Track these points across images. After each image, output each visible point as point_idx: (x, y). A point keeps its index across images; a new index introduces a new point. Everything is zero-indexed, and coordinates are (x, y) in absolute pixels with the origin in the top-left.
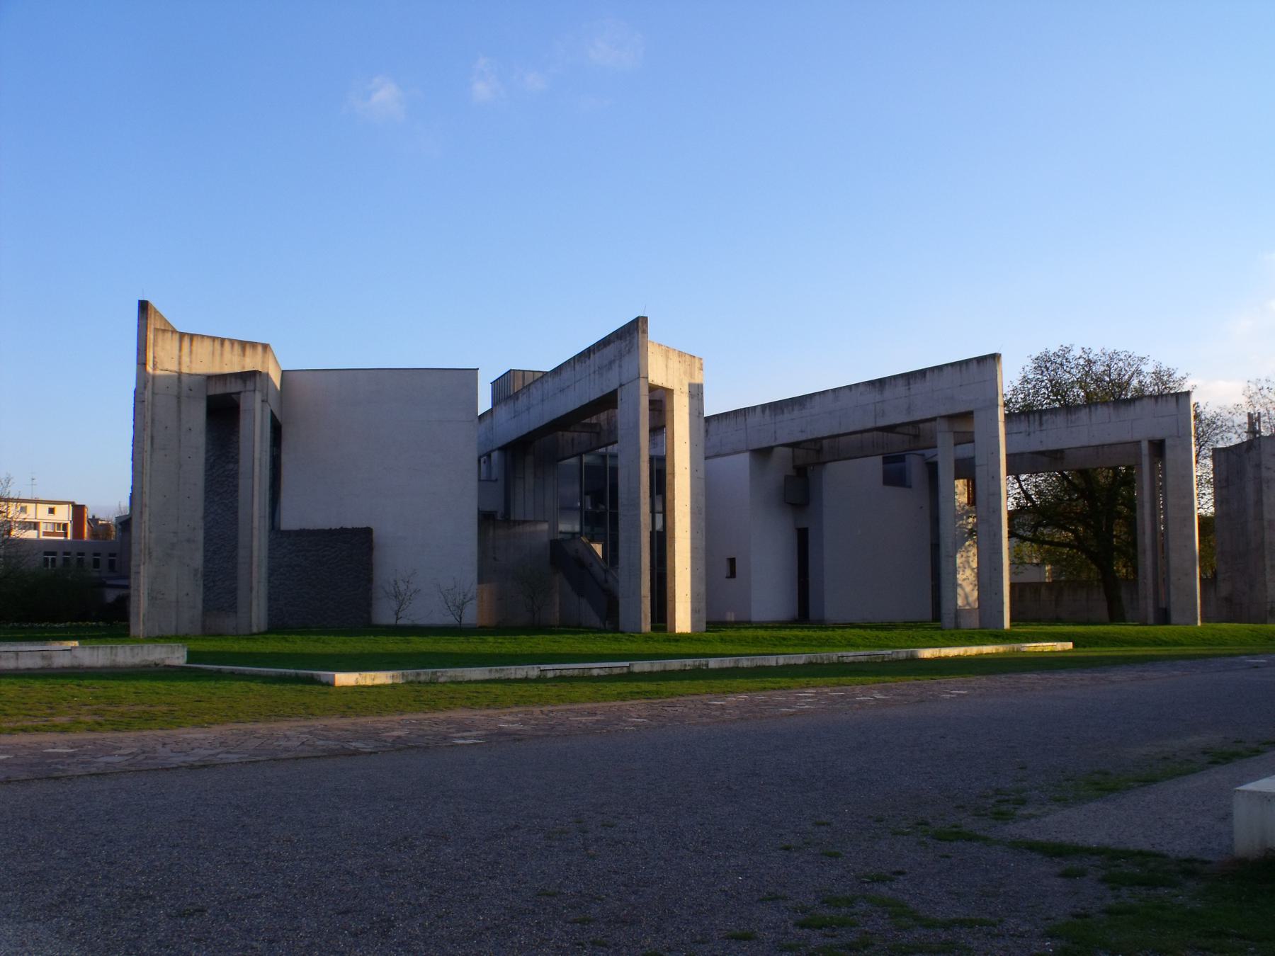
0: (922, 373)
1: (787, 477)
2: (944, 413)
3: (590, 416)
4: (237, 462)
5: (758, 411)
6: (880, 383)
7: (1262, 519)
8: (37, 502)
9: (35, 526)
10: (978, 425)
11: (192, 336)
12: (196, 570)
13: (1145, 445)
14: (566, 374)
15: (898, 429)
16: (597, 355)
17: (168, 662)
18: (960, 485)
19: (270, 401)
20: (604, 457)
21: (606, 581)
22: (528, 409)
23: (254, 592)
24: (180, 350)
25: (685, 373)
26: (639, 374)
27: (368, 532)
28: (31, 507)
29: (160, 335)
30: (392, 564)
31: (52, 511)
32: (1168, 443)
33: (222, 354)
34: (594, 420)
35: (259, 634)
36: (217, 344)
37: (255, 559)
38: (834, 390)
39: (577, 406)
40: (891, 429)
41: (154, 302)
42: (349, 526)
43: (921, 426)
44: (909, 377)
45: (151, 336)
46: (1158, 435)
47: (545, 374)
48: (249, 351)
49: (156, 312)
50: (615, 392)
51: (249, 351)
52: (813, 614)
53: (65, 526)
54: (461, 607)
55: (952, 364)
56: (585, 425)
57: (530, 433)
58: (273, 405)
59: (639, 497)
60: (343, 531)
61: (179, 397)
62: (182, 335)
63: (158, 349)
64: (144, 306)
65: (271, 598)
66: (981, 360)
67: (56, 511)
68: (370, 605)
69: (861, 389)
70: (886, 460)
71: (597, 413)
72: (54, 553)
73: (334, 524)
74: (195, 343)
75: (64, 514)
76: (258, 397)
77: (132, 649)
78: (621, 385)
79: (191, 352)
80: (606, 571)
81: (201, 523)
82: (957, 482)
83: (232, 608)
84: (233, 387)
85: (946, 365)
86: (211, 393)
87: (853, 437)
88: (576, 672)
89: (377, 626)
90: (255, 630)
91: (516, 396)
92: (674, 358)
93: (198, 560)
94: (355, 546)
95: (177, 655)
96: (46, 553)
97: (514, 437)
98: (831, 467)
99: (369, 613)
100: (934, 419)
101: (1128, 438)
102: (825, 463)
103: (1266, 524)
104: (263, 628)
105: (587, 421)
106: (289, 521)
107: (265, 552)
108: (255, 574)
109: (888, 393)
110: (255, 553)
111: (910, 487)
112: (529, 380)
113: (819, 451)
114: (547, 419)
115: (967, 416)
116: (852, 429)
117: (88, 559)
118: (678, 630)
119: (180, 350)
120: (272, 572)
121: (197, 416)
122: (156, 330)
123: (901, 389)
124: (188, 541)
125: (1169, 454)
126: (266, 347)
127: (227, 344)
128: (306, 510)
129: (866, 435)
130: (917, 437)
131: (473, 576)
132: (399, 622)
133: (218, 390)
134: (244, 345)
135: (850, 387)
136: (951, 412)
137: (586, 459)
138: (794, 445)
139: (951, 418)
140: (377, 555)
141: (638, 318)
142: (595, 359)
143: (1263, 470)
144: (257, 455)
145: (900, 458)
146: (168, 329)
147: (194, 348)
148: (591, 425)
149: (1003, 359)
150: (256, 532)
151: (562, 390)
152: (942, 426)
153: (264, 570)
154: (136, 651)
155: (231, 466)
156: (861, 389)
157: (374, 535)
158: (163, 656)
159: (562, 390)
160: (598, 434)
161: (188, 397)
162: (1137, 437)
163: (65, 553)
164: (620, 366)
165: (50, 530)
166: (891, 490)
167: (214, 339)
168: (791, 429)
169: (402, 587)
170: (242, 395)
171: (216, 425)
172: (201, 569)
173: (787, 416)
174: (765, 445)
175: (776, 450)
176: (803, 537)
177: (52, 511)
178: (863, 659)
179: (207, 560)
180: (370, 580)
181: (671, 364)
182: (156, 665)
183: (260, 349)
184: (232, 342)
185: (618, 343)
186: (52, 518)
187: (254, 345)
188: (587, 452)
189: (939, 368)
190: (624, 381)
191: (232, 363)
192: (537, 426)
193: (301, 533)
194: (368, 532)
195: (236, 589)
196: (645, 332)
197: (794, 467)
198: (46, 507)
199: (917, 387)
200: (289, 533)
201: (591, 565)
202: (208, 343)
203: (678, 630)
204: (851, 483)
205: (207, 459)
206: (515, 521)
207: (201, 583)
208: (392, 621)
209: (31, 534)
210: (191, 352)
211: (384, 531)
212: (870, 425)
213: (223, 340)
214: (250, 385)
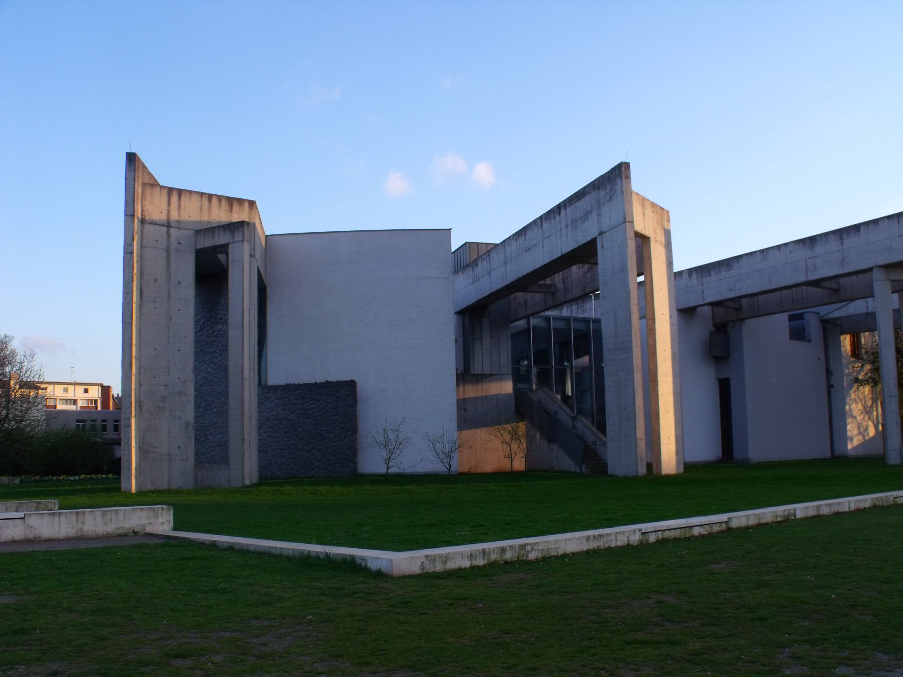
0: (856, 228)
1: (711, 333)
3: (544, 278)
4: (226, 323)
6: (811, 241)
8: (75, 384)
9: (75, 402)
11: (180, 192)
12: (187, 423)
14: (529, 234)
16: (569, 209)
17: (149, 529)
18: (569, 391)
19: (257, 256)
20: (548, 319)
21: (575, 428)
22: (489, 273)
23: (246, 446)
24: (169, 204)
25: (657, 222)
26: (626, 220)
27: (352, 384)
28: (71, 388)
29: (148, 189)
30: (376, 416)
31: (86, 391)
33: (209, 209)
34: (548, 281)
35: (252, 486)
36: (205, 200)
37: (246, 410)
38: (762, 251)
41: (143, 157)
42: (334, 380)
43: (841, 280)
44: (841, 233)
45: (139, 189)
48: (236, 207)
49: (144, 167)
50: (594, 241)
51: (236, 207)
52: (738, 455)
53: (96, 401)
54: (449, 456)
56: (541, 286)
58: (259, 262)
59: (630, 341)
60: (328, 384)
61: (167, 250)
62: (170, 190)
63: (147, 203)
64: (132, 159)
65: (261, 451)
67: (89, 391)
68: (355, 455)
69: (791, 247)
70: (791, 318)
72: (84, 421)
74: (183, 198)
75: (95, 393)
76: (246, 246)
77: (104, 514)
78: (601, 233)
79: (179, 206)
80: (573, 418)
81: (191, 376)
82: (842, 338)
83: (224, 459)
84: (221, 239)
86: (200, 246)
88: (677, 533)
89: (363, 476)
90: (247, 482)
91: (475, 263)
93: (189, 412)
94: (335, 404)
95: (160, 519)
96: (78, 421)
99: (355, 463)
100: (870, 270)
102: (744, 320)
104: (255, 480)
106: (276, 377)
107: (255, 405)
108: (246, 426)
109: (819, 249)
110: (246, 405)
111: (810, 341)
112: (489, 247)
113: (739, 309)
114: (556, 255)
116: (782, 285)
117: (99, 423)
119: (169, 204)
120: (261, 425)
121: (185, 270)
122: (144, 184)
123: (833, 245)
124: (179, 393)
126: (252, 203)
127: (215, 201)
128: (291, 365)
129: (784, 292)
131: (454, 423)
133: (206, 242)
134: (231, 201)
138: (713, 304)
140: (360, 407)
142: (569, 212)
144: (246, 305)
145: (800, 317)
146: (154, 184)
147: (182, 202)
150: (246, 383)
151: (528, 249)
153: (254, 422)
154: (109, 516)
155: (220, 327)
156: (791, 247)
158: (144, 521)
159: (528, 249)
160: (553, 294)
161: (177, 250)
163: (92, 421)
164: (599, 215)
165: (85, 405)
167: (202, 194)
170: (230, 247)
171: (203, 272)
172: (192, 421)
173: (714, 277)
175: (699, 309)
176: (725, 388)
177: (86, 391)
179: (198, 416)
180: (355, 431)
181: (646, 211)
182: (135, 533)
183: (246, 205)
184: (220, 197)
185: (594, 194)
186: (87, 396)
187: (241, 201)
188: (533, 315)
190: (605, 228)
191: (220, 215)
192: (499, 287)
193: (288, 387)
194: (352, 384)
195: (227, 442)
196: (628, 177)
198: (82, 388)
199: (851, 241)
200: (276, 388)
201: (556, 413)
202: (195, 198)
203: (664, 472)
204: (766, 335)
205: (196, 322)
206: (476, 375)
207: (192, 435)
208: (382, 470)
209: (72, 408)
210: (179, 206)
213: (210, 196)
214: (238, 236)
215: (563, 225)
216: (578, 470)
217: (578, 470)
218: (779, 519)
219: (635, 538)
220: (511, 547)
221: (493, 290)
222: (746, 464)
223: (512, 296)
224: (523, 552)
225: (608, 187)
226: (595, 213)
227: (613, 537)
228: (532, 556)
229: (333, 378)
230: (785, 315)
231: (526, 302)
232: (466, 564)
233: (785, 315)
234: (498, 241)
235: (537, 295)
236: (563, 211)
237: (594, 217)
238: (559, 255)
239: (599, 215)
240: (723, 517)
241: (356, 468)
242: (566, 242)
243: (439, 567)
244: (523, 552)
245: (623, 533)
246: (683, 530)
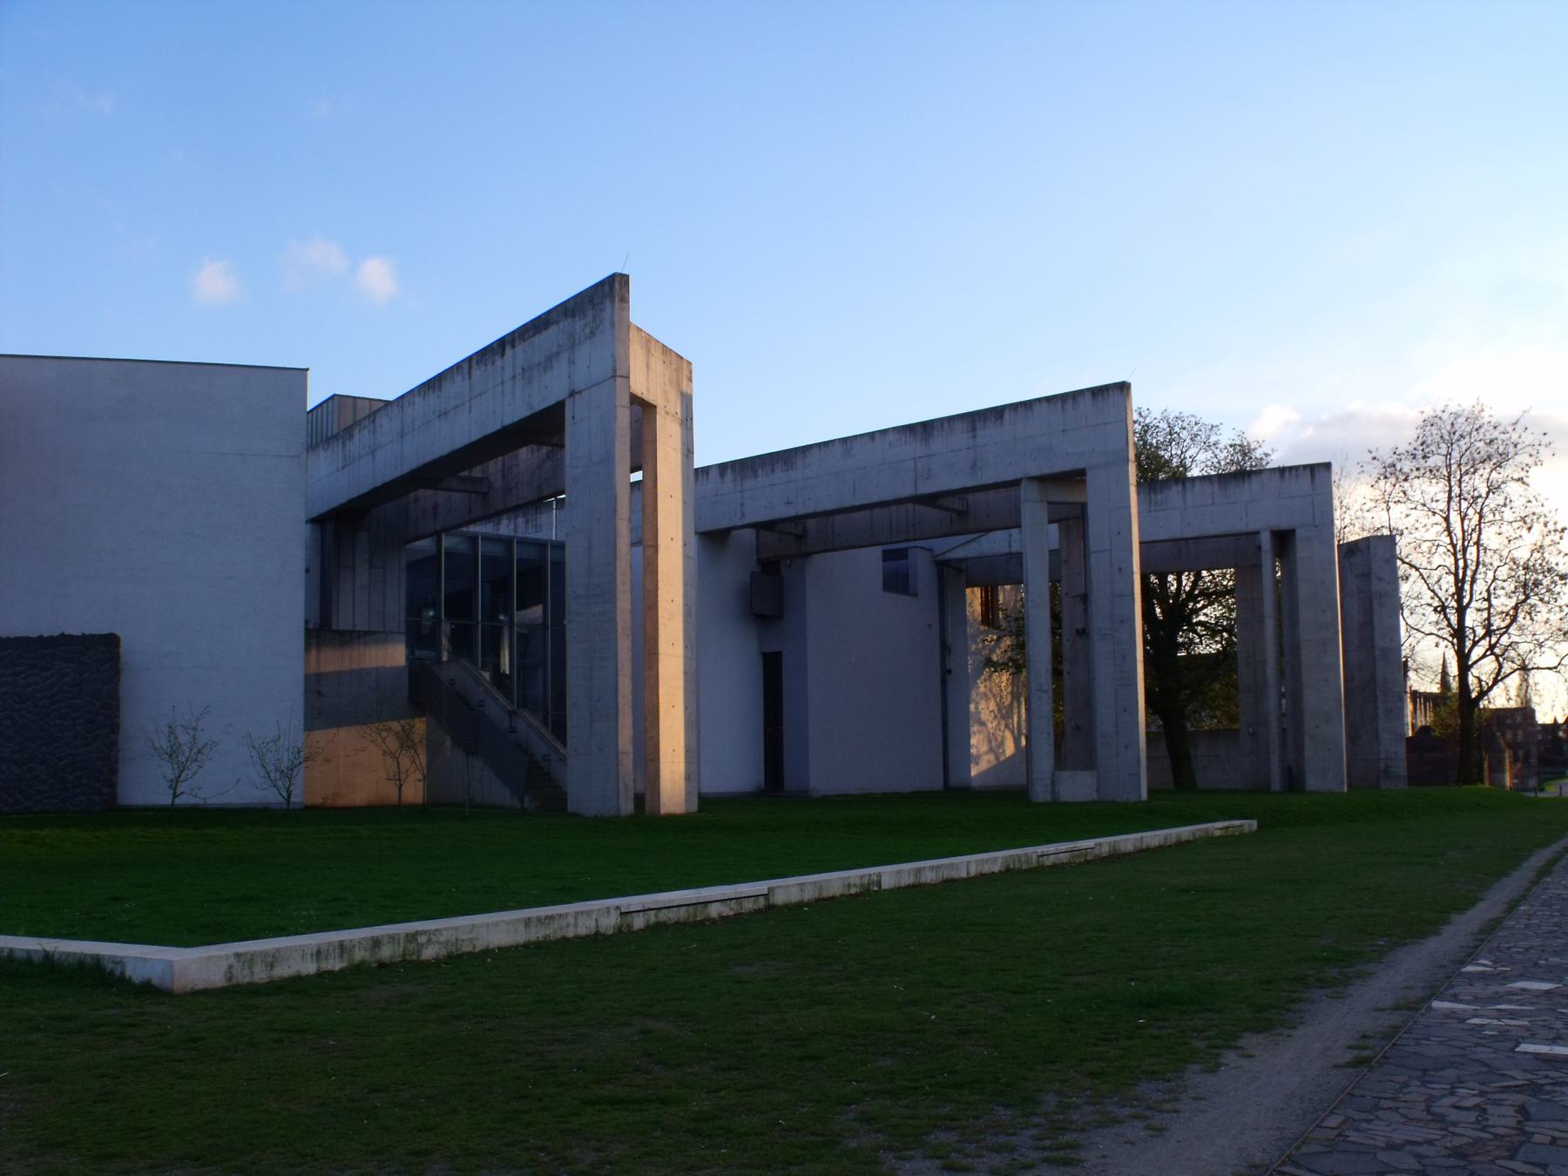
0: (998, 413)
1: (753, 574)
2: (1034, 472)
5: (714, 474)
7: (1373, 646)
10: (1094, 495)
13: (1266, 540)
14: (448, 388)
15: (945, 502)
16: (519, 348)
20: (473, 539)
21: (513, 730)
22: (373, 452)
26: (617, 373)
30: (153, 704)
32: (1300, 534)
34: (477, 472)
38: (844, 440)
39: (475, 436)
40: (931, 500)
43: (970, 497)
44: (974, 419)
46: (1285, 525)
47: (387, 403)
50: (559, 407)
52: (790, 782)
54: (287, 774)
55: (1049, 399)
57: (350, 502)
60: (64, 640)
66: (1098, 392)
68: (114, 771)
69: (891, 437)
70: (888, 556)
71: (483, 460)
73: (49, 629)
78: (572, 394)
80: (511, 714)
85: (1039, 400)
87: (856, 515)
89: (129, 809)
92: (657, 356)
97: (343, 501)
98: (818, 560)
100: (1016, 483)
101: (1241, 527)
102: (809, 554)
103: (1377, 652)
105: (465, 473)
106: (699, 462)
109: (937, 443)
111: (916, 595)
112: (376, 406)
113: (801, 537)
115: (1076, 477)
118: (664, 810)
125: (1301, 551)
129: (878, 512)
130: (962, 514)
131: (298, 718)
132: (178, 801)
135: (872, 435)
136: (1046, 471)
137: (447, 542)
138: (758, 526)
139: (1045, 480)
140: (125, 680)
141: (613, 277)
143: (1374, 581)
145: (902, 554)
148: (473, 480)
149: (1134, 391)
152: (1028, 492)
157: (124, 647)
160: (485, 495)
162: (1252, 527)
164: (572, 362)
166: (892, 598)
168: (768, 502)
169: (184, 738)
174: (724, 524)
176: (772, 669)
178: (1064, 858)
185: (565, 324)
188: (447, 530)
189: (1027, 405)
190: (579, 385)
192: (388, 478)
196: (625, 300)
197: (759, 561)
199: (987, 433)
201: (481, 703)
203: (664, 810)
204: (846, 584)
206: (341, 633)
208: (164, 799)
211: (140, 645)
212: (908, 491)
215: (508, 374)
216: (516, 803)
217: (516, 803)
218: (853, 891)
219: (609, 923)
220: (392, 938)
221: (379, 482)
222: (804, 798)
223: (412, 495)
224: (411, 946)
225: (590, 314)
226: (564, 358)
227: (571, 920)
228: (429, 953)
229: (75, 630)
230: (877, 552)
231: (435, 507)
232: (310, 968)
233: (877, 552)
234: (391, 396)
235: (456, 496)
236: (508, 351)
237: (562, 364)
238: (498, 427)
239: (572, 362)
240: (760, 887)
241: (114, 795)
242: (510, 405)
243: (260, 975)
244: (411, 946)
245: (589, 913)
246: (691, 909)
